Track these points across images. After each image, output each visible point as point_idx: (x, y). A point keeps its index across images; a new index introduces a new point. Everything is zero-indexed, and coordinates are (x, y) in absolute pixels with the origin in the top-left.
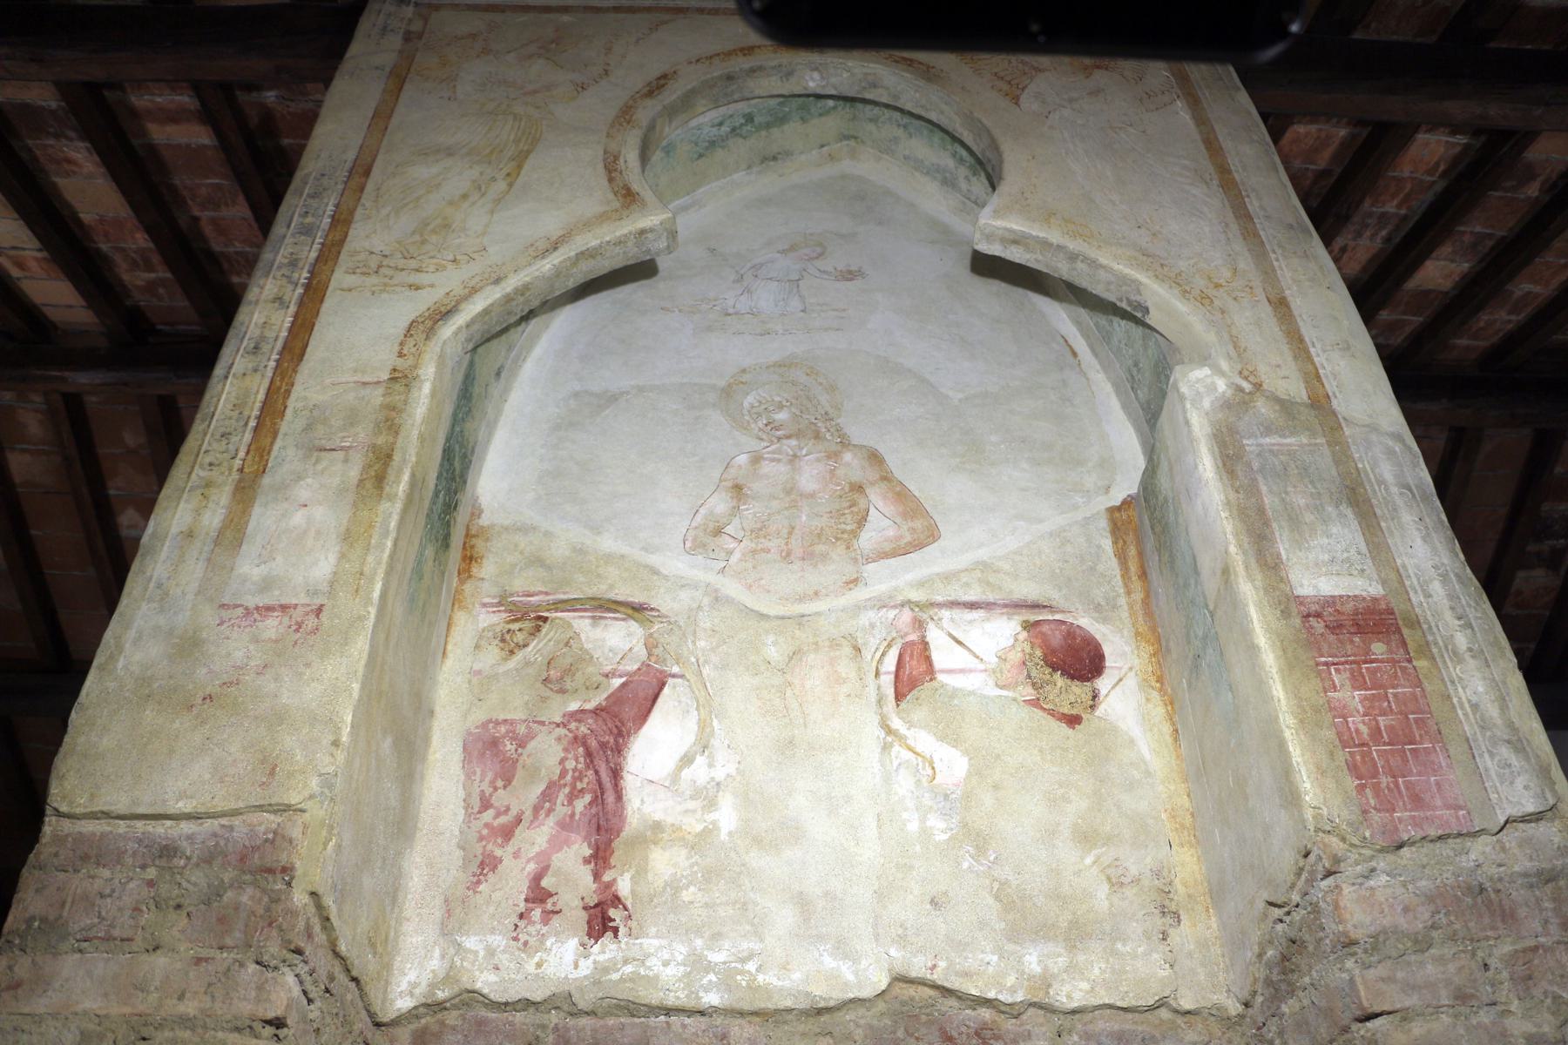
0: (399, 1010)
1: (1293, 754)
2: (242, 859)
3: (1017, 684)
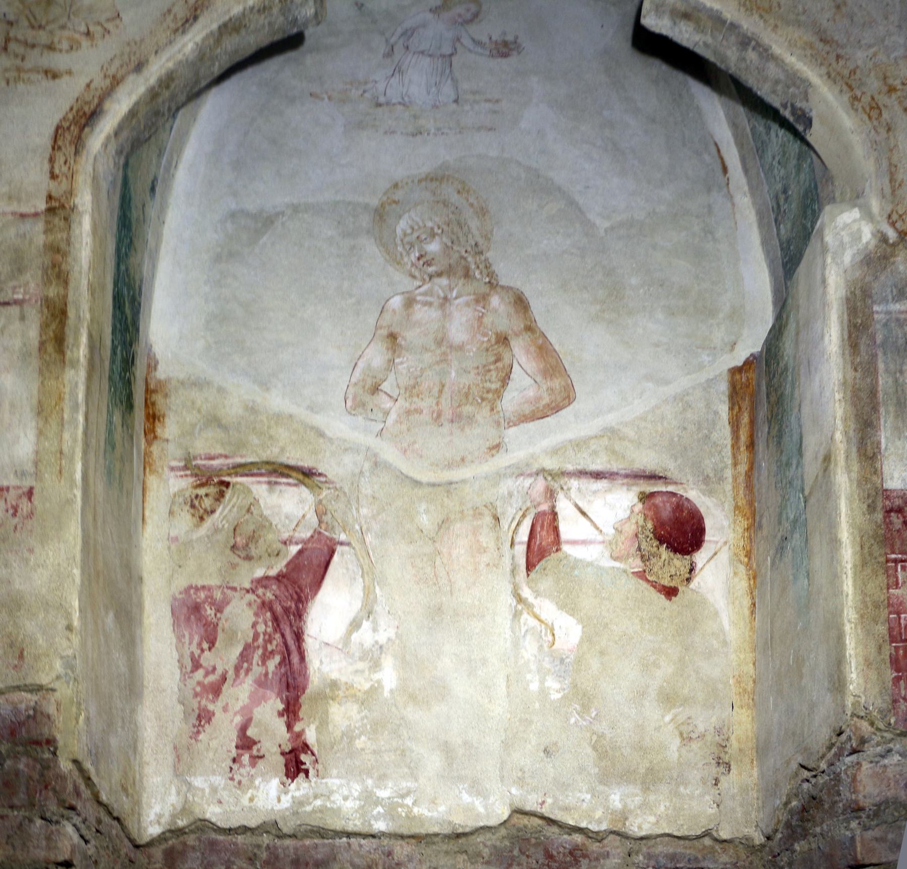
0: (151, 835)
1: (848, 647)
2: (13, 733)
3: (628, 556)
